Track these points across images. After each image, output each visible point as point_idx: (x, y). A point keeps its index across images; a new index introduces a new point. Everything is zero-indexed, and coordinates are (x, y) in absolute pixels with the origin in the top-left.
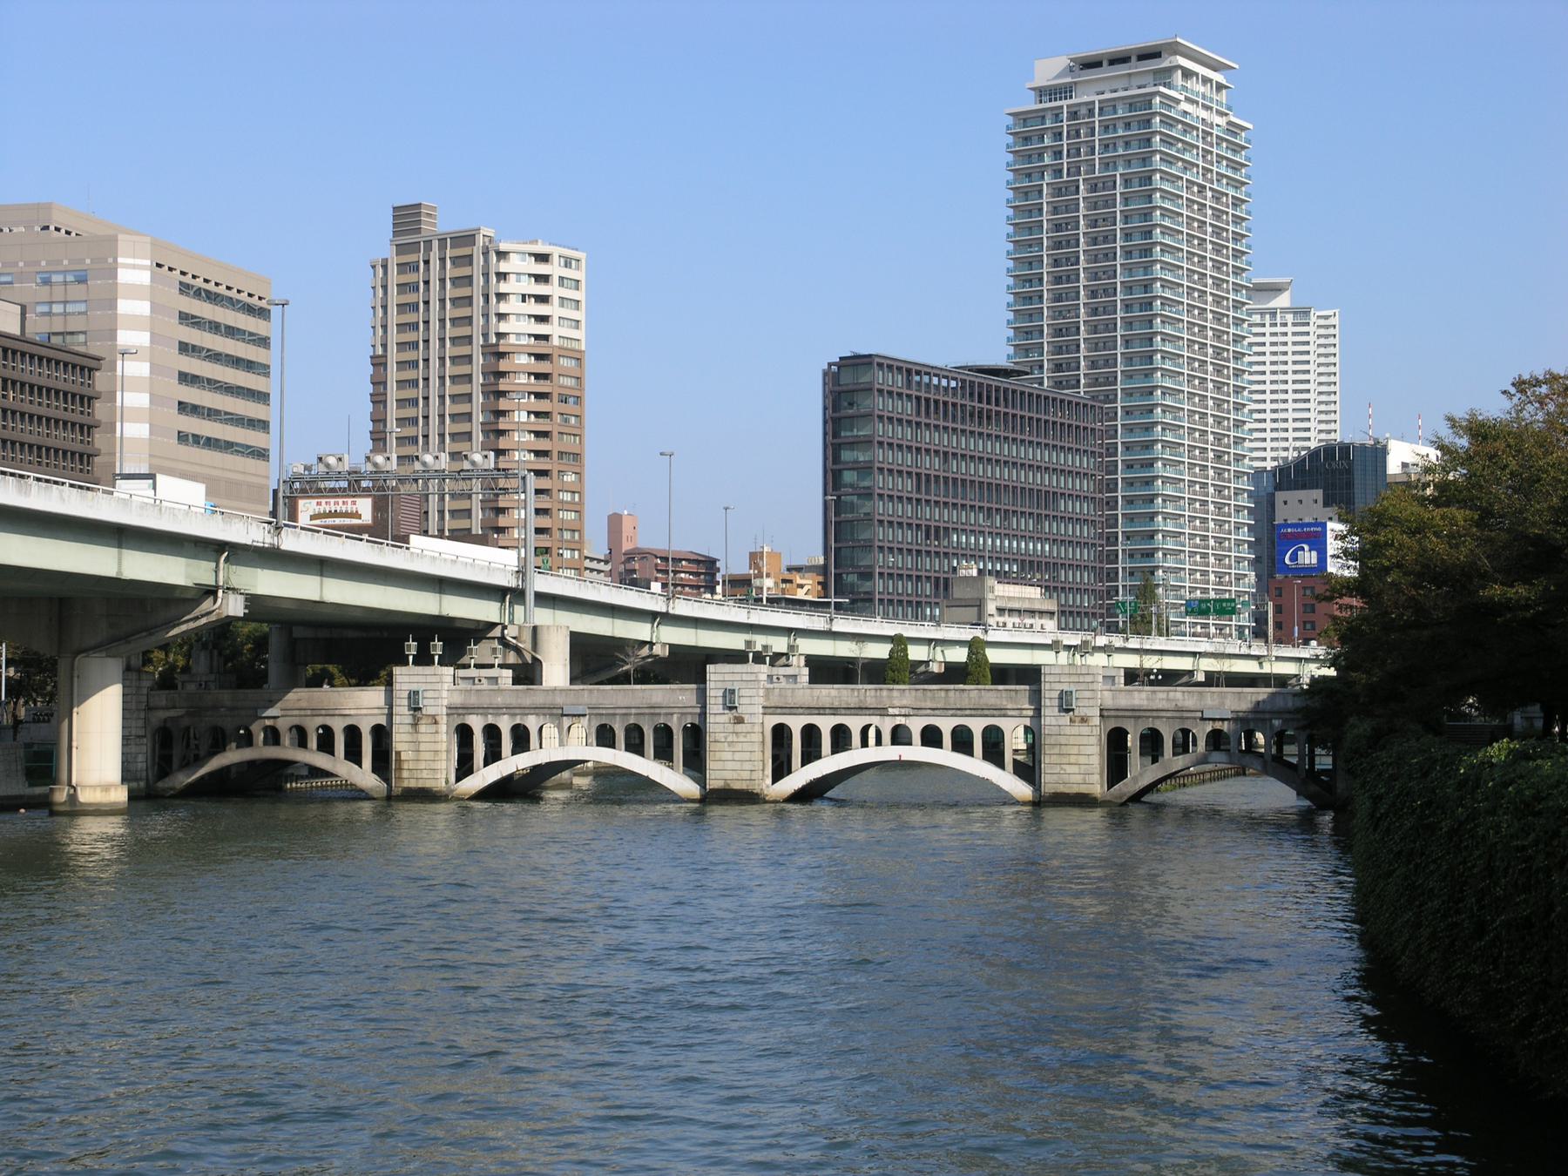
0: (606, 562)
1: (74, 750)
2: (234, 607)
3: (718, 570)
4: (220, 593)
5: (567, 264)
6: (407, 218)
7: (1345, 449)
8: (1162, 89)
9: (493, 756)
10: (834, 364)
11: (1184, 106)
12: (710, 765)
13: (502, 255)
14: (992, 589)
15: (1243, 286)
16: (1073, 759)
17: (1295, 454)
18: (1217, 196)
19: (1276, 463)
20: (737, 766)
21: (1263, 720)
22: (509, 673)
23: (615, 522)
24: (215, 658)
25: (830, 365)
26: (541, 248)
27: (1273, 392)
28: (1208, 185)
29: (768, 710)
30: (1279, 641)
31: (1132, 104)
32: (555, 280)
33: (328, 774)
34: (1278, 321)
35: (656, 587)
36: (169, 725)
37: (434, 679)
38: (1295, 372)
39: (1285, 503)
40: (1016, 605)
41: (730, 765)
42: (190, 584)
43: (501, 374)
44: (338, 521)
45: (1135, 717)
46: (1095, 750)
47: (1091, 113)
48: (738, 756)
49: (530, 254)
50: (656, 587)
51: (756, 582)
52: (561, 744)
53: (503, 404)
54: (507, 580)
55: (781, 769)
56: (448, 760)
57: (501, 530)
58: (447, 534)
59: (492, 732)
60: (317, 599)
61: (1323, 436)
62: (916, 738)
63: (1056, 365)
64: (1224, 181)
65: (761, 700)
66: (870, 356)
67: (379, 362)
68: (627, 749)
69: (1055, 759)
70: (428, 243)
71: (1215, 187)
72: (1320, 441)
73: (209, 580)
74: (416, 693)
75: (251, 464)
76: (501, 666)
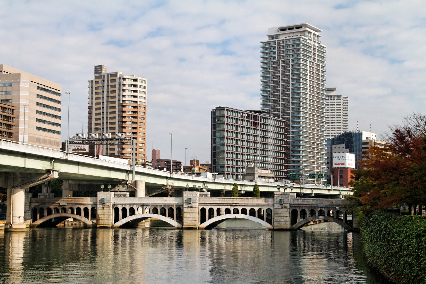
0: (151, 162)
1: (105, 226)
2: (55, 175)
3: (182, 165)
4: (52, 171)
5: (142, 82)
6: (98, 69)
7: (351, 133)
8: (302, 36)
9: (124, 216)
10: (214, 109)
11: (308, 41)
12: (184, 219)
13: (124, 79)
14: (257, 171)
15: (324, 89)
16: (282, 218)
17: (338, 135)
18: (318, 65)
19: (332, 137)
20: (191, 219)
21: (334, 207)
22: (128, 193)
23: (154, 152)
24: (49, 189)
25: (213, 110)
26: (135, 77)
27: (331, 118)
28: (315, 62)
29: (200, 204)
30: (334, 185)
31: (294, 40)
32: (139, 86)
33: (79, 221)
34: (333, 99)
35: (165, 169)
36: (36, 207)
37: (108, 195)
38: (337, 113)
39: (335, 148)
40: (263, 175)
41: (189, 219)
42: (43, 169)
43: (124, 112)
44: (79, 151)
45: (299, 206)
46: (288, 215)
47: (283, 42)
48: (191, 216)
49: (132, 79)
50: (165, 169)
51: (193, 169)
52: (143, 213)
53: (124, 120)
54: (128, 168)
55: (203, 220)
56: (112, 217)
57: (123, 154)
58: (108, 155)
59: (124, 210)
60: (77, 173)
61: (345, 130)
62: (240, 212)
63: (274, 110)
64: (319, 61)
65: (198, 202)
66: (224, 107)
67: (90, 108)
68: (161, 214)
69: (277, 218)
70: (104, 76)
71: (316, 63)
72: (344, 131)
73: (48, 168)
74: (104, 199)
75: (56, 135)
76: (127, 192)
